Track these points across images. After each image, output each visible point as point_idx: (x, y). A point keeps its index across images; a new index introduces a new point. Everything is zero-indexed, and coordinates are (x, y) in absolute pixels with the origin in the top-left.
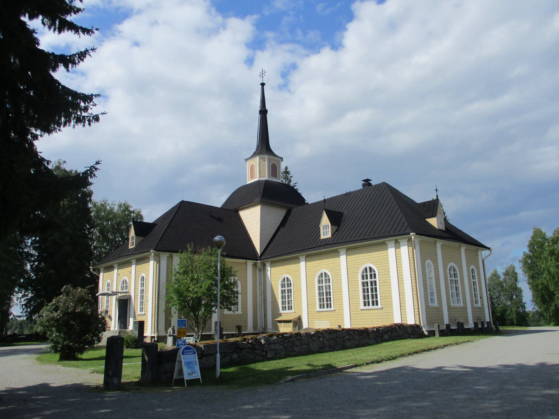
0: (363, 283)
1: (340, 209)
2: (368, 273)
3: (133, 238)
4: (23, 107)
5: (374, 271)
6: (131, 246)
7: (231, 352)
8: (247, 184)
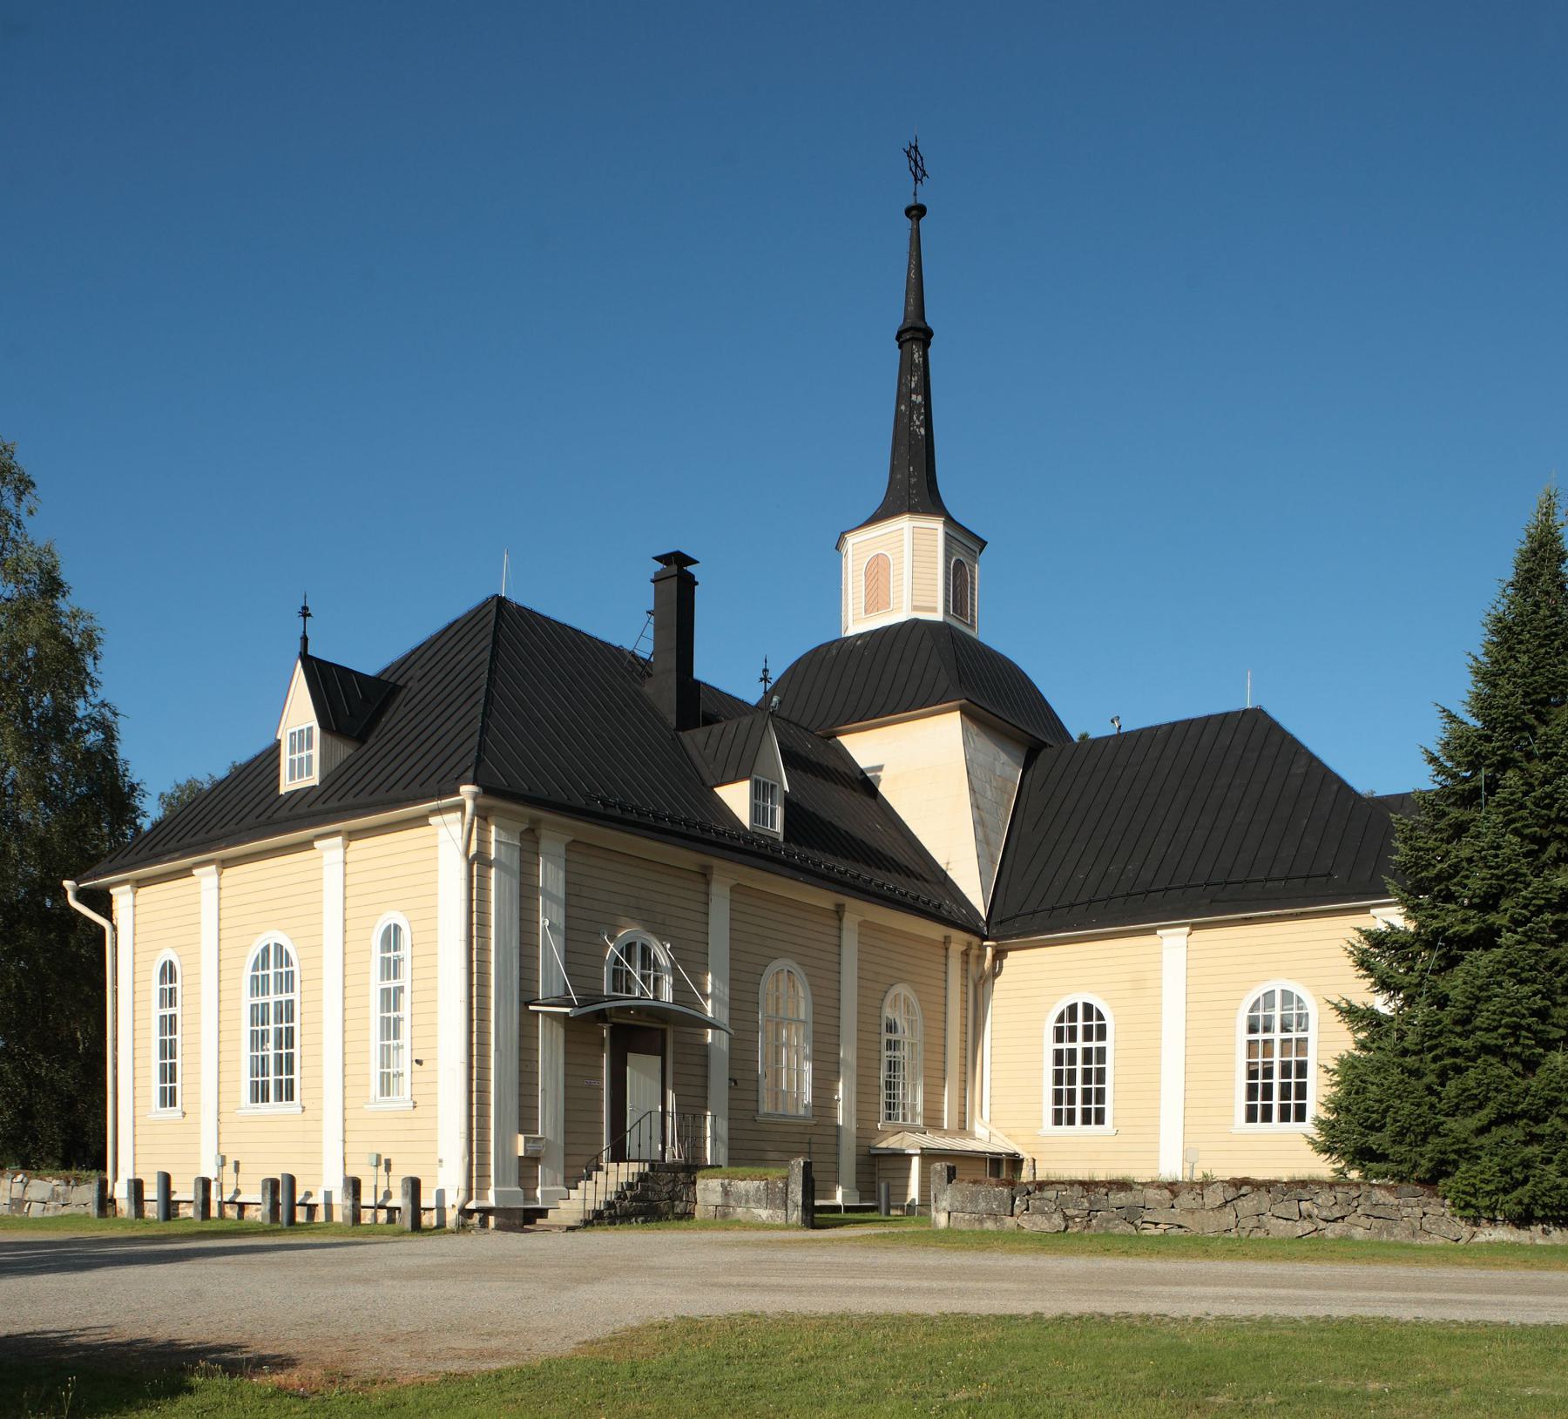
0: (1058, 1055)
1: (397, 675)
2: (1080, 1023)
3: (303, 738)
4: (918, 427)
5: (1100, 1017)
6: (292, 777)
7: (1479, 1033)
8: (857, 621)
